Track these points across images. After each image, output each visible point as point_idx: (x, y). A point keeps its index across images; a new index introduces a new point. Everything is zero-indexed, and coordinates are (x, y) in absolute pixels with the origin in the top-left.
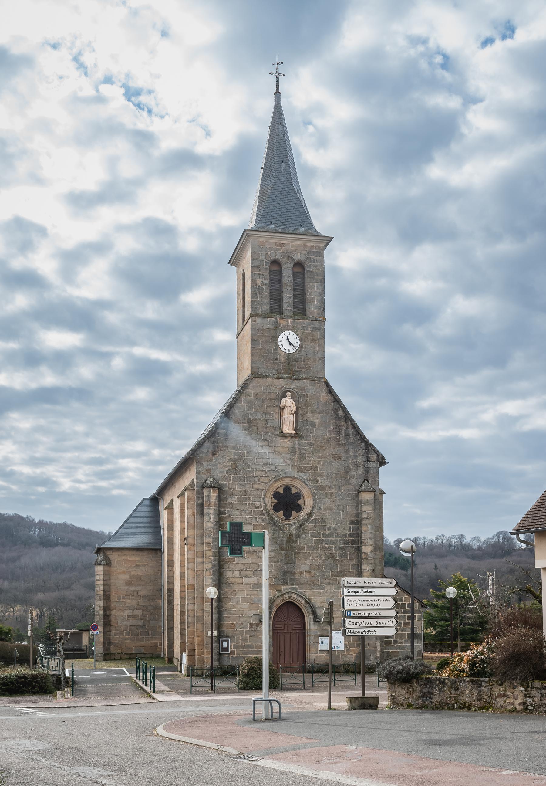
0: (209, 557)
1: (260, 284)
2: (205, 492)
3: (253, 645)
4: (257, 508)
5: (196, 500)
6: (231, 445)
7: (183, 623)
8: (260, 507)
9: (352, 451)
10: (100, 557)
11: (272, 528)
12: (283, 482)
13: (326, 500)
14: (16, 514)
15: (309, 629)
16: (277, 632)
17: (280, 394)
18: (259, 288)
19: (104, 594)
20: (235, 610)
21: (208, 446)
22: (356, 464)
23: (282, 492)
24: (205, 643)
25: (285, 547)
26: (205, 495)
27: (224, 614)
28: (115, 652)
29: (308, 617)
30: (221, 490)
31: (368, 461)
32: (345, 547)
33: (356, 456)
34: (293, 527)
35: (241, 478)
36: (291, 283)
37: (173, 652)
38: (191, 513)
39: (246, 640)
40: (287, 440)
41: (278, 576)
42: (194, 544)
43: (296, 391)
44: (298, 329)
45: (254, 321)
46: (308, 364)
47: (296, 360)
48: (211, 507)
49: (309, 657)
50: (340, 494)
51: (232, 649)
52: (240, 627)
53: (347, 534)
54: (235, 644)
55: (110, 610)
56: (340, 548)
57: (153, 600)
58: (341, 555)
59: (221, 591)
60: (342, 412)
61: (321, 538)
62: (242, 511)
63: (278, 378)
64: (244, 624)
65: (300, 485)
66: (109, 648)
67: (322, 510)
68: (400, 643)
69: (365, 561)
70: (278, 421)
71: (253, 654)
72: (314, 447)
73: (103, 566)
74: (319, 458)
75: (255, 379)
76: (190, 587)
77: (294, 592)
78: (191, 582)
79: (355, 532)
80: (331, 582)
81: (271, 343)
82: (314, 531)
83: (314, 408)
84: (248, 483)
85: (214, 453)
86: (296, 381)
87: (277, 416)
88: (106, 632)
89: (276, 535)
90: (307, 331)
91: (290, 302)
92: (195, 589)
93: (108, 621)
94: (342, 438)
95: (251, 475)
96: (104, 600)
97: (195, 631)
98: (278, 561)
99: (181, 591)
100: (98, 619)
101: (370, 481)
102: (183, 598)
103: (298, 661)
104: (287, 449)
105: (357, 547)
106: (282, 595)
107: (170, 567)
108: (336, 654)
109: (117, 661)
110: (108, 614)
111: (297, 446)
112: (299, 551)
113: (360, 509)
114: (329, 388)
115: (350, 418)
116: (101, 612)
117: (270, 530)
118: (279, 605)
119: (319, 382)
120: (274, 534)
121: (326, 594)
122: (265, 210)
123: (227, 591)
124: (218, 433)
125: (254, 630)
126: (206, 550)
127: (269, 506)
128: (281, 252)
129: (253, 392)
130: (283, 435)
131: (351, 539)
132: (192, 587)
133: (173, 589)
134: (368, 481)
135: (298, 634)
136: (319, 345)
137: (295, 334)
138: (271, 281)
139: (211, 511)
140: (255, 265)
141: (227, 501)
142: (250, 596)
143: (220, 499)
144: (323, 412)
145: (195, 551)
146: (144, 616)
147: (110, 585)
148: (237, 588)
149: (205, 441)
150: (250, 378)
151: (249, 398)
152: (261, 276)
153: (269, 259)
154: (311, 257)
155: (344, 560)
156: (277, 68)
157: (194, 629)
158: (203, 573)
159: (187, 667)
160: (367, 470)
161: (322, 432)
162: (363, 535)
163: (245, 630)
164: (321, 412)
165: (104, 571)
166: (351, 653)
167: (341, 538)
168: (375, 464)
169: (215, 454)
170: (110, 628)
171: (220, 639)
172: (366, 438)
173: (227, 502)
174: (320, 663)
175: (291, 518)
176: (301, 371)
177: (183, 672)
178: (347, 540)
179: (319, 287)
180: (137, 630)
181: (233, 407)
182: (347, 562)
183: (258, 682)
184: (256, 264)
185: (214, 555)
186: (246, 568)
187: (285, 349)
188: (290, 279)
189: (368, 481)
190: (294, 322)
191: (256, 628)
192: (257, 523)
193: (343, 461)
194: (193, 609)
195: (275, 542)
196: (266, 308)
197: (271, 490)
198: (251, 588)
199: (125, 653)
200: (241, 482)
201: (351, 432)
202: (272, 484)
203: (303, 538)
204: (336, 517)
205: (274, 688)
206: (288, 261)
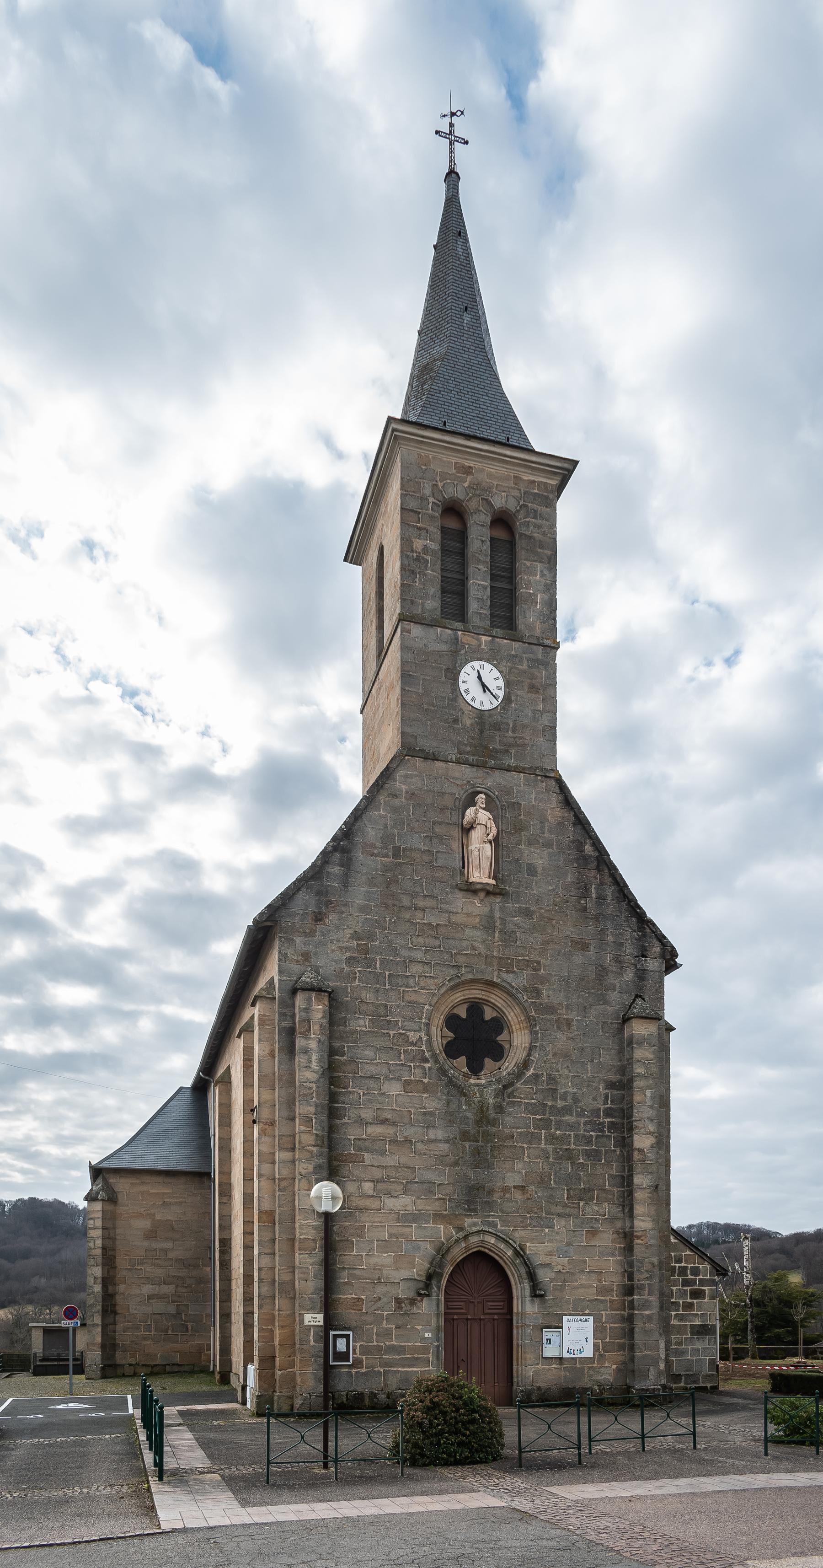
0: (308, 1148)
1: (420, 550)
2: (300, 1000)
3: (404, 1347)
4: (412, 1044)
5: (279, 1020)
6: (357, 901)
7: (248, 1299)
8: (419, 1043)
9: (612, 934)
10: (97, 1186)
11: (445, 1091)
12: (467, 992)
13: (558, 1034)
14: (56, 1200)
15: (520, 1311)
16: (453, 1319)
17: (463, 797)
18: (418, 559)
19: (103, 1255)
20: (363, 1269)
21: (304, 897)
22: (619, 962)
23: (464, 1015)
24: (298, 1342)
25: (472, 1132)
26: (299, 1008)
27: (340, 1278)
28: (124, 1362)
29: (519, 1286)
30: (333, 999)
31: (643, 956)
32: (597, 1137)
33: (619, 945)
34: (489, 1090)
35: (378, 977)
36: (486, 555)
37: (230, 1361)
38: (267, 1051)
39: (388, 1334)
40: (476, 901)
41: (455, 1197)
42: (275, 1121)
43: (496, 793)
44: (502, 660)
45: (407, 632)
46: (521, 738)
47: (497, 727)
48: (313, 1036)
49: (520, 1372)
50: (587, 1025)
51: (358, 1355)
52: (375, 1307)
53: (599, 1109)
54: (365, 1344)
55: (115, 1284)
56: (586, 1139)
57: (196, 1266)
58: (588, 1154)
59: (334, 1226)
60: (591, 849)
61: (547, 1116)
62: (380, 1049)
63: (458, 762)
64: (384, 1300)
65: (502, 1002)
66: (113, 1356)
67: (550, 1056)
68: (677, 1343)
69: (638, 1168)
70: (458, 857)
71: (404, 1366)
72: (533, 919)
73: (101, 1202)
74: (544, 943)
75: (408, 759)
76: (265, 1217)
77: (490, 1230)
78: (266, 1207)
79: (617, 1106)
80: (568, 1211)
81: (443, 683)
82: (533, 1101)
83: (533, 835)
84: (393, 989)
85: (319, 918)
86: (497, 773)
87: (456, 846)
88: (107, 1325)
89: (454, 1106)
90: (520, 667)
91: (485, 598)
92: (274, 1220)
93: (111, 1304)
94: (590, 904)
95: (399, 970)
96: (104, 1265)
97: (274, 1315)
98: (456, 1163)
99: (245, 1233)
100: (92, 1301)
101: (646, 998)
102: (248, 1248)
103: (496, 1381)
104: (477, 920)
105: (620, 1138)
106: (466, 1237)
107: (225, 1196)
108: (578, 1365)
109: (127, 1379)
110: (110, 1290)
111: (497, 915)
112: (500, 1143)
113: (627, 1057)
114: (565, 794)
115: (607, 861)
116: (98, 1288)
117: (439, 1094)
118: (458, 1260)
119: (543, 779)
120: (448, 1103)
121: (558, 1237)
122: (430, 396)
123: (345, 1227)
124: (328, 873)
125: (405, 1314)
126: (300, 1132)
127: (438, 1045)
128: (466, 484)
129: (404, 788)
130: (471, 889)
131: (609, 1120)
132: (268, 1217)
133: (230, 1239)
134: (643, 999)
135: (496, 1322)
136: (544, 699)
137: (495, 670)
138: (444, 549)
139: (313, 1045)
140: (410, 507)
141: (346, 1026)
142: (398, 1238)
143: (333, 1019)
144: (553, 845)
145: (274, 1137)
146: (179, 1296)
147: (116, 1239)
148: (367, 1219)
149: (299, 889)
150: (399, 756)
151: (396, 802)
152: (423, 533)
153: (441, 498)
154: (529, 505)
155: (593, 1166)
156: (451, 125)
157: (274, 1309)
158: (294, 1185)
159: (258, 1396)
160: (641, 975)
161: (550, 888)
162: (635, 1111)
163: (385, 1313)
164: (548, 845)
165: (103, 1211)
166: (607, 1364)
167: (589, 1117)
168: (656, 964)
169: (320, 920)
170: (115, 1318)
171: (332, 1333)
172: (640, 908)
173: (348, 1028)
174: (544, 1385)
175: (482, 1073)
176: (507, 751)
177: (248, 1406)
178: (600, 1124)
179: (546, 572)
180: (165, 1322)
181: (360, 816)
182: (599, 1170)
183: (452, 1444)
184: (413, 504)
185: (319, 1143)
186: (389, 1177)
187: (473, 699)
188: (485, 547)
189: (643, 999)
190: (492, 642)
191: (409, 1308)
192: (412, 1078)
193: (592, 953)
194: (270, 1265)
195: (450, 1121)
196: (432, 604)
197: (442, 1009)
198: (398, 1220)
199: (143, 1363)
200: (378, 986)
201: (610, 891)
202: (443, 995)
203: (510, 1114)
204: (578, 1073)
205: (495, 1459)
206: (481, 508)
